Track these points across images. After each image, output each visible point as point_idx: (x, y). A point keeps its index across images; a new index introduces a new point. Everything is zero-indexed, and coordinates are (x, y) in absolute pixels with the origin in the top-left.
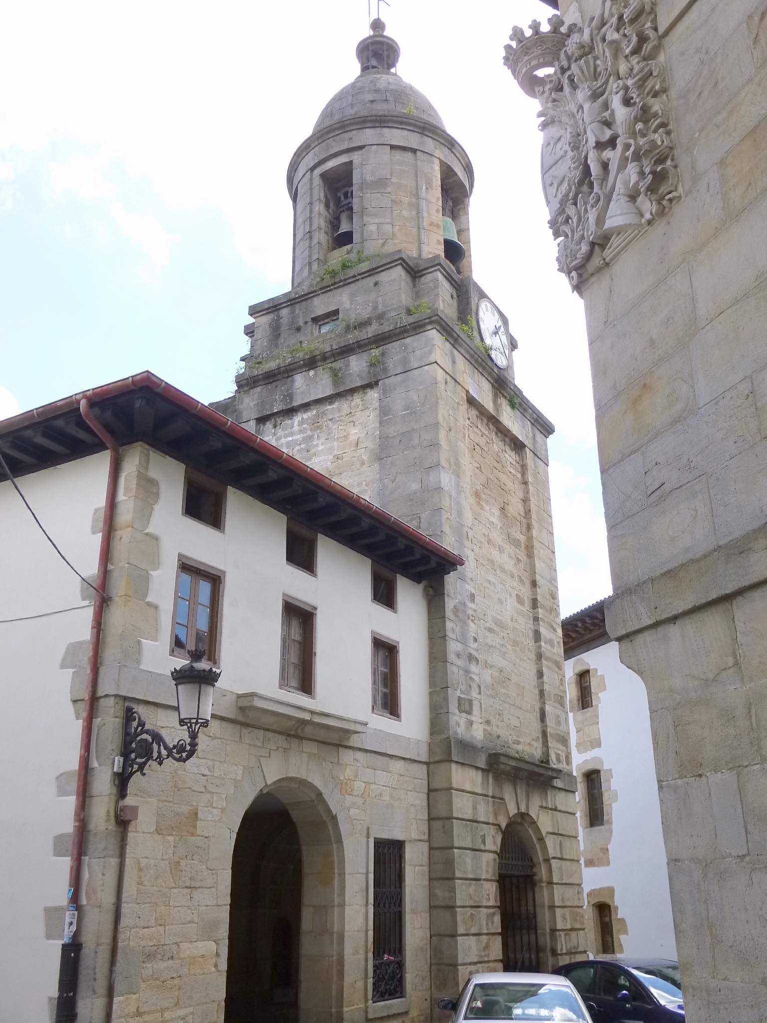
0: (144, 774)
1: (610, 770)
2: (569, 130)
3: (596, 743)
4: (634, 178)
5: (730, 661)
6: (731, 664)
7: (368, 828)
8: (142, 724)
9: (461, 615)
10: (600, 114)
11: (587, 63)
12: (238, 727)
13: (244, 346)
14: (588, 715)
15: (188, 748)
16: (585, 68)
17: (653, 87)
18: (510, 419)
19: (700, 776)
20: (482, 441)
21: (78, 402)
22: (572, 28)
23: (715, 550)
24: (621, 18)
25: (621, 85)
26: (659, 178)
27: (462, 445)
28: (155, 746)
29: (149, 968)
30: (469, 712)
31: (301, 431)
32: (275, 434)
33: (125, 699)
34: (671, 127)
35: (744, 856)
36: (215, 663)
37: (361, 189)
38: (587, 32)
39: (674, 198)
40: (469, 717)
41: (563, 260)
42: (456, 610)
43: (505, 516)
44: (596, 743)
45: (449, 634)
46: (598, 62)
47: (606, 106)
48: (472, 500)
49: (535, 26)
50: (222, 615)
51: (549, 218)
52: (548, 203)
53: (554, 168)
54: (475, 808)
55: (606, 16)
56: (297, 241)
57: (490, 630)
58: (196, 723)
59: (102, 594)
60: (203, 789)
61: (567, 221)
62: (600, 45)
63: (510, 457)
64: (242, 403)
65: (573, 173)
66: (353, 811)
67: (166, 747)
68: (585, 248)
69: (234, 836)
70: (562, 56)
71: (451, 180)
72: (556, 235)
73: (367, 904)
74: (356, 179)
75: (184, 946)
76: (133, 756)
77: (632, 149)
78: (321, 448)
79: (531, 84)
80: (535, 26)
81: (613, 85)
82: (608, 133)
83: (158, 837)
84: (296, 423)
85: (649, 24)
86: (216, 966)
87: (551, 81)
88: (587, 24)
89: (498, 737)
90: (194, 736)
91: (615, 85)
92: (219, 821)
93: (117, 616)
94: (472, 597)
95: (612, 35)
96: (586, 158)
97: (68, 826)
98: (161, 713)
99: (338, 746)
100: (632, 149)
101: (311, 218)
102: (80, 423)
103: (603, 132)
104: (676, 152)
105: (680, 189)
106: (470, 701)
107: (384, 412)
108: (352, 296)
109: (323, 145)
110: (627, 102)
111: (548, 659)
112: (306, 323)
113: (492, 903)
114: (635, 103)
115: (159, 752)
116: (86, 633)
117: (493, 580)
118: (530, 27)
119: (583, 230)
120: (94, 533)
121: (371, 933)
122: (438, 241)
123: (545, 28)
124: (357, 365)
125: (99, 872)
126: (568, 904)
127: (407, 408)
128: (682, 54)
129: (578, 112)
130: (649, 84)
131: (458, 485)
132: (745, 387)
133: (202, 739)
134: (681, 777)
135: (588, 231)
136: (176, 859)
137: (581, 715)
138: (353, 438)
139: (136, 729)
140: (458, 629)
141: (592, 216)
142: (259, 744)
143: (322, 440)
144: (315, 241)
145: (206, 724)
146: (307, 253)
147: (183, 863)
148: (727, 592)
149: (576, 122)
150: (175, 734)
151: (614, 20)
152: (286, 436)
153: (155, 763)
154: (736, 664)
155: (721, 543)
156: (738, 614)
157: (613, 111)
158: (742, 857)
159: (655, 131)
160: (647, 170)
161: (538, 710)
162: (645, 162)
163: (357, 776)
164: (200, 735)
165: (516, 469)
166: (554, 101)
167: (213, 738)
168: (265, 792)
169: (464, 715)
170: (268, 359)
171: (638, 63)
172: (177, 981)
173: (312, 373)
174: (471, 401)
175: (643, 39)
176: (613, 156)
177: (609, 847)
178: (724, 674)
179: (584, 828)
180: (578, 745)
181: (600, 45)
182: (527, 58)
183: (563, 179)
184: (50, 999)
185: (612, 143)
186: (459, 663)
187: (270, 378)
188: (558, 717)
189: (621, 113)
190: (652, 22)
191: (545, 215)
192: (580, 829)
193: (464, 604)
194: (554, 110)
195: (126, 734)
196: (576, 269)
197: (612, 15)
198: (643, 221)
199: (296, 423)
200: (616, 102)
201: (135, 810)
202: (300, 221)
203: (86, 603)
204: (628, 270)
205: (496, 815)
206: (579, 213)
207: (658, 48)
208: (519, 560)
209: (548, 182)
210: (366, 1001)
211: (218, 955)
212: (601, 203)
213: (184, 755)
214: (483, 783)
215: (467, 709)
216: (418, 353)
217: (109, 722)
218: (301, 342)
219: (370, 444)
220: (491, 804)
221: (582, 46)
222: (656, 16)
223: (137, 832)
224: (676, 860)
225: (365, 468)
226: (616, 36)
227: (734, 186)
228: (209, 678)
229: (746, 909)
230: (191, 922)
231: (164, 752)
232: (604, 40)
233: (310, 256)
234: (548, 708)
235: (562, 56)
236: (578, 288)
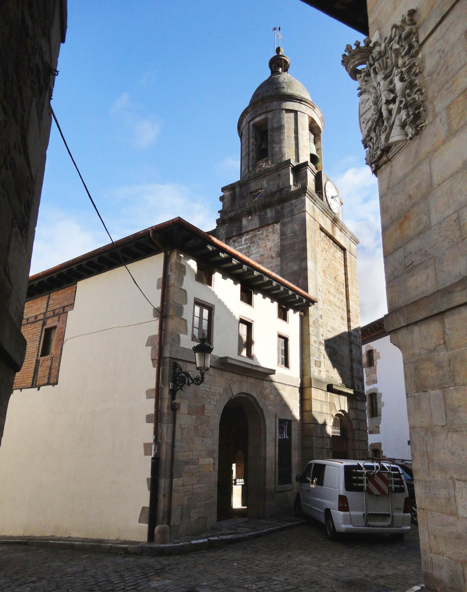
0: (182, 390)
1: (381, 393)
2: (373, 95)
3: (375, 382)
4: (404, 117)
5: (442, 342)
6: (442, 343)
7: (276, 415)
8: (181, 369)
9: (316, 324)
10: (388, 86)
11: (383, 61)
12: (221, 371)
13: (220, 206)
14: (372, 369)
15: (200, 379)
16: (381, 64)
17: (416, 71)
18: (339, 236)
19: (426, 392)
20: (327, 247)
21: (149, 232)
22: (376, 44)
23: (437, 292)
24: (400, 37)
25: (399, 71)
26: (417, 117)
27: (317, 249)
28: (187, 379)
29: (186, 468)
30: (320, 367)
31: (246, 244)
32: (234, 245)
33: (174, 359)
34: (423, 91)
35: (444, 426)
36: (211, 344)
37: (272, 131)
38: (383, 45)
39: (423, 126)
40: (319, 369)
41: (368, 158)
42: (314, 322)
43: (337, 281)
44: (375, 382)
45: (311, 332)
46: (388, 60)
47: (391, 82)
48: (322, 274)
49: (357, 44)
50: (213, 323)
51: (362, 139)
52: (362, 131)
53: (365, 115)
54: (322, 407)
55: (393, 36)
56: (243, 156)
57: (329, 331)
58: (204, 369)
59: (163, 314)
60: (207, 397)
61: (370, 140)
62: (389, 51)
63: (340, 254)
64: (219, 232)
65: (374, 117)
66: (269, 407)
67: (191, 379)
68: (379, 152)
69: (220, 416)
70: (370, 59)
71: (313, 125)
72: (366, 147)
73: (275, 446)
74: (269, 126)
75: (201, 460)
76: (177, 382)
77: (404, 103)
78: (254, 251)
79: (354, 74)
80: (357, 44)
81: (395, 71)
82: (392, 96)
83: (189, 416)
84: (243, 240)
85: (414, 39)
86: (214, 468)
87: (365, 71)
88: (383, 41)
89: (332, 377)
90: (203, 374)
91: (396, 72)
92: (214, 410)
93: (172, 324)
94: (321, 317)
95: (396, 46)
96: (381, 108)
97: (152, 411)
98: (188, 365)
99: (263, 380)
100: (404, 103)
101: (249, 146)
102: (150, 240)
103: (389, 96)
104: (427, 103)
105: (427, 122)
106: (320, 362)
107: (282, 234)
108: (268, 182)
109: (254, 110)
110: (402, 80)
111: (355, 344)
112: (247, 194)
113: (328, 447)
114: (406, 80)
115: (188, 381)
116: (156, 332)
117: (330, 309)
118: (355, 44)
119: (378, 144)
120: (158, 289)
121: (277, 457)
122: (307, 154)
123: (362, 45)
124: (270, 213)
125: (166, 429)
126: (362, 448)
127: (293, 232)
128: (430, 54)
129: (377, 86)
130: (414, 69)
131: (315, 267)
132: (454, 217)
133: (206, 376)
134: (417, 392)
135: (381, 144)
136: (196, 425)
137: (368, 370)
138: (268, 247)
139: (178, 371)
140: (315, 331)
141: (383, 137)
142: (229, 378)
143: (255, 248)
144: (251, 156)
145: (208, 369)
146: (247, 162)
147: (199, 427)
148: (442, 311)
149: (377, 91)
150: (195, 374)
151: (397, 38)
152: (239, 246)
153: (187, 386)
154: (445, 343)
155: (440, 289)
156: (446, 321)
157: (395, 84)
158: (443, 426)
159: (415, 93)
160: (411, 113)
161: (349, 366)
162: (409, 109)
163: (271, 393)
164: (205, 374)
165: (342, 260)
166: (366, 81)
167: (211, 376)
168: (232, 398)
169: (317, 368)
170: (230, 212)
171: (408, 59)
172: (198, 474)
173: (250, 217)
174: (322, 229)
175: (411, 47)
176: (394, 107)
177: (380, 426)
178: (439, 347)
179: (369, 418)
180: (367, 382)
181: (389, 51)
182: (353, 60)
183: (370, 119)
184: (148, 479)
185: (393, 101)
186: (316, 345)
187: (232, 220)
188: (358, 369)
189: (399, 85)
190: (416, 38)
191: (360, 137)
192: (367, 418)
193: (318, 320)
194: (366, 86)
195: (174, 373)
196: (374, 163)
197: (395, 36)
198: (408, 138)
199: (243, 240)
200: (396, 80)
201: (179, 404)
202: (244, 147)
203: (156, 319)
204: (399, 164)
205: (331, 410)
206: (376, 135)
207: (417, 53)
208: (342, 300)
209: (362, 121)
210: (275, 484)
211: (214, 464)
212: (387, 130)
213: (199, 382)
214: (325, 397)
215: (319, 365)
216: (298, 207)
217: (168, 368)
218: (245, 203)
219: (276, 249)
220: (328, 406)
221: (380, 53)
222: (418, 35)
223: (180, 414)
224: (413, 427)
225: (274, 260)
226: (397, 46)
227: (454, 119)
228: (210, 350)
229: (444, 448)
230: (203, 450)
231: (190, 381)
232: (391, 49)
233: (248, 164)
234: (354, 366)
235: (370, 59)
236: (375, 172)
